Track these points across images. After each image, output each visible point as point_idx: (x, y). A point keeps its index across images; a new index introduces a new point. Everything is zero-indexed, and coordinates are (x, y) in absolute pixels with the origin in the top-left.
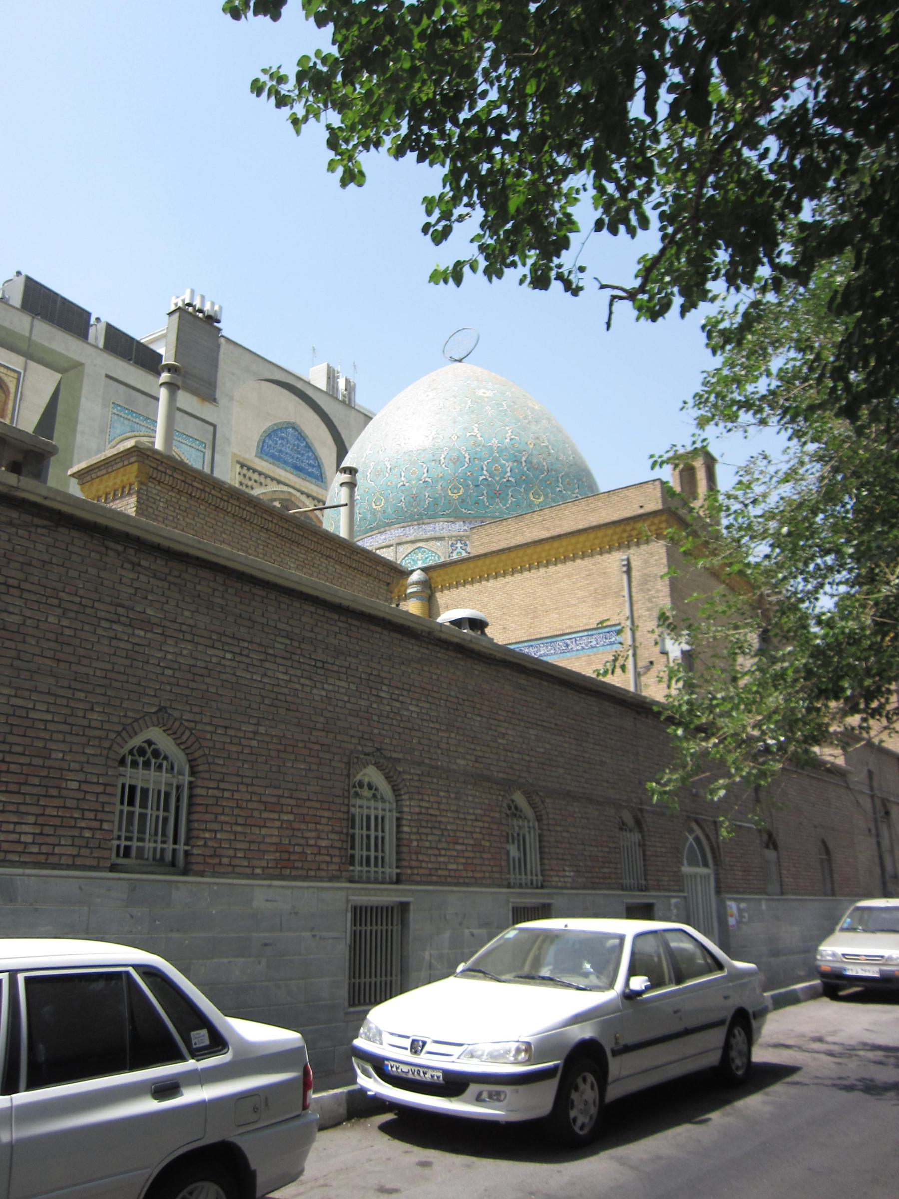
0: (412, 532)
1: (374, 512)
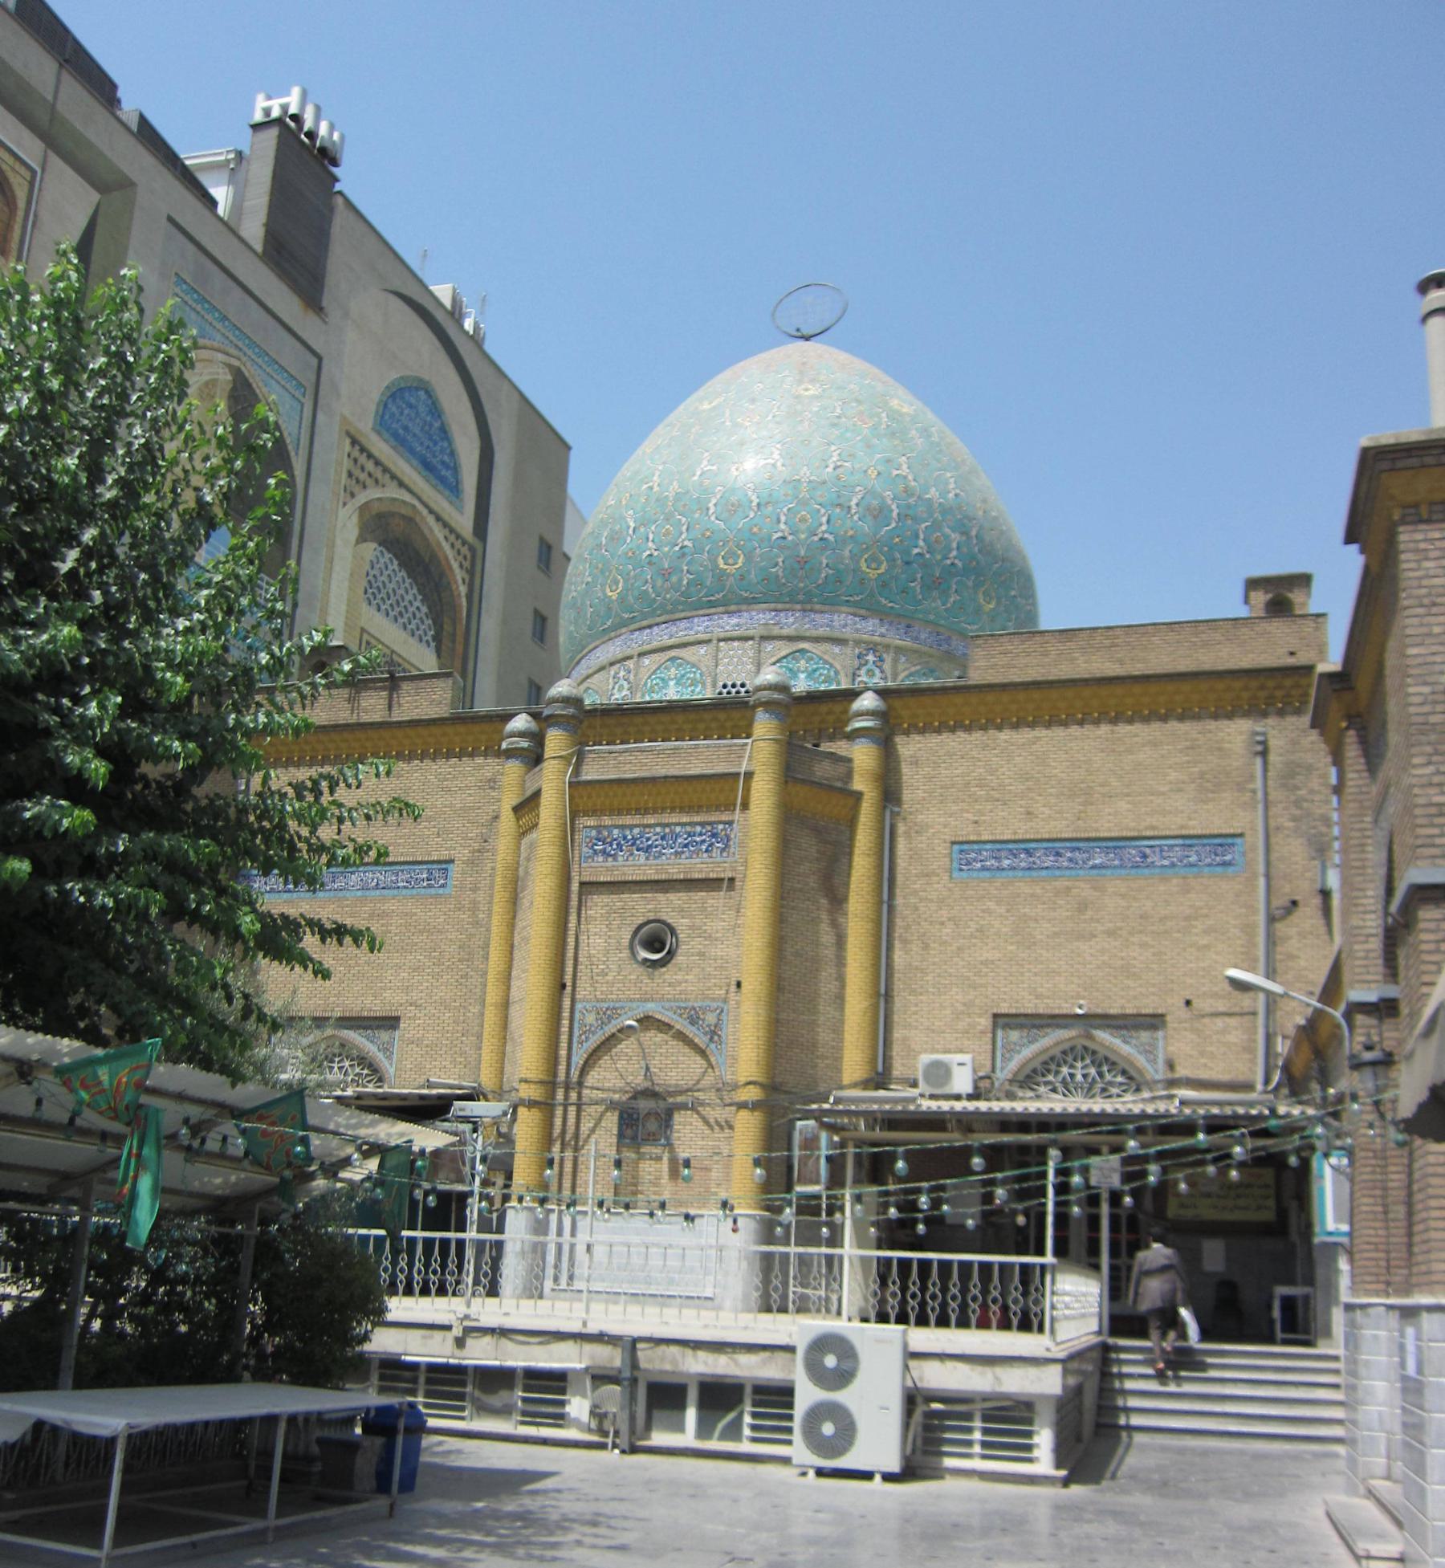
0: (790, 623)
1: (721, 576)
